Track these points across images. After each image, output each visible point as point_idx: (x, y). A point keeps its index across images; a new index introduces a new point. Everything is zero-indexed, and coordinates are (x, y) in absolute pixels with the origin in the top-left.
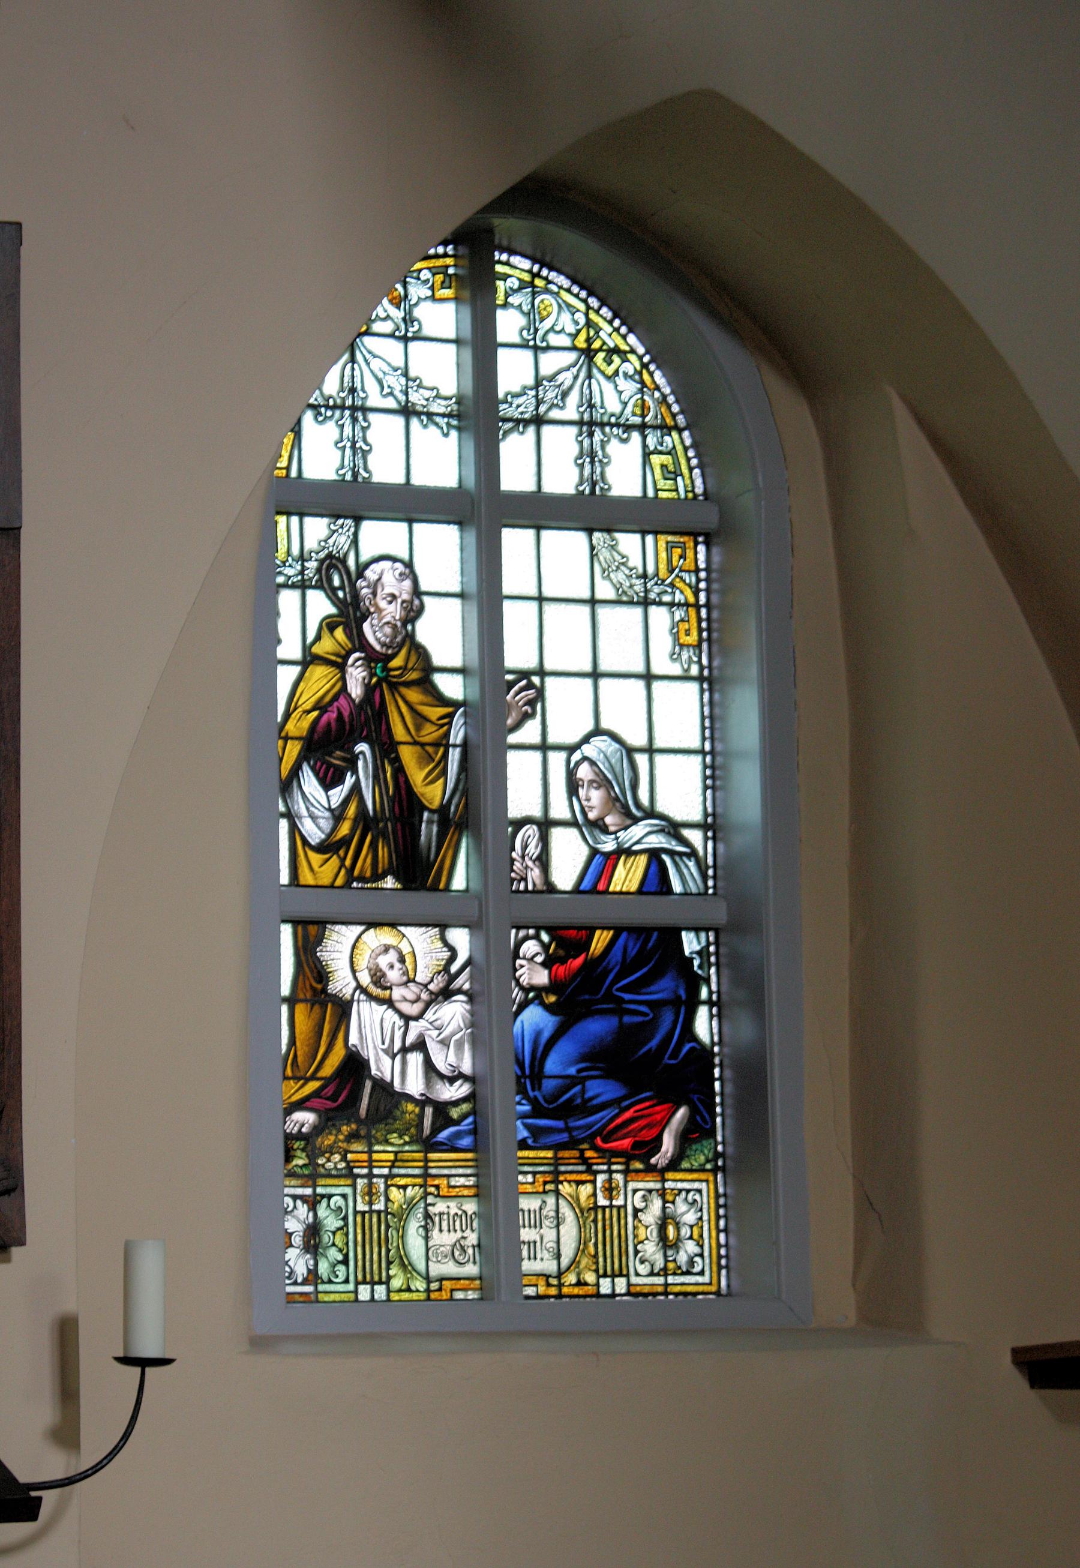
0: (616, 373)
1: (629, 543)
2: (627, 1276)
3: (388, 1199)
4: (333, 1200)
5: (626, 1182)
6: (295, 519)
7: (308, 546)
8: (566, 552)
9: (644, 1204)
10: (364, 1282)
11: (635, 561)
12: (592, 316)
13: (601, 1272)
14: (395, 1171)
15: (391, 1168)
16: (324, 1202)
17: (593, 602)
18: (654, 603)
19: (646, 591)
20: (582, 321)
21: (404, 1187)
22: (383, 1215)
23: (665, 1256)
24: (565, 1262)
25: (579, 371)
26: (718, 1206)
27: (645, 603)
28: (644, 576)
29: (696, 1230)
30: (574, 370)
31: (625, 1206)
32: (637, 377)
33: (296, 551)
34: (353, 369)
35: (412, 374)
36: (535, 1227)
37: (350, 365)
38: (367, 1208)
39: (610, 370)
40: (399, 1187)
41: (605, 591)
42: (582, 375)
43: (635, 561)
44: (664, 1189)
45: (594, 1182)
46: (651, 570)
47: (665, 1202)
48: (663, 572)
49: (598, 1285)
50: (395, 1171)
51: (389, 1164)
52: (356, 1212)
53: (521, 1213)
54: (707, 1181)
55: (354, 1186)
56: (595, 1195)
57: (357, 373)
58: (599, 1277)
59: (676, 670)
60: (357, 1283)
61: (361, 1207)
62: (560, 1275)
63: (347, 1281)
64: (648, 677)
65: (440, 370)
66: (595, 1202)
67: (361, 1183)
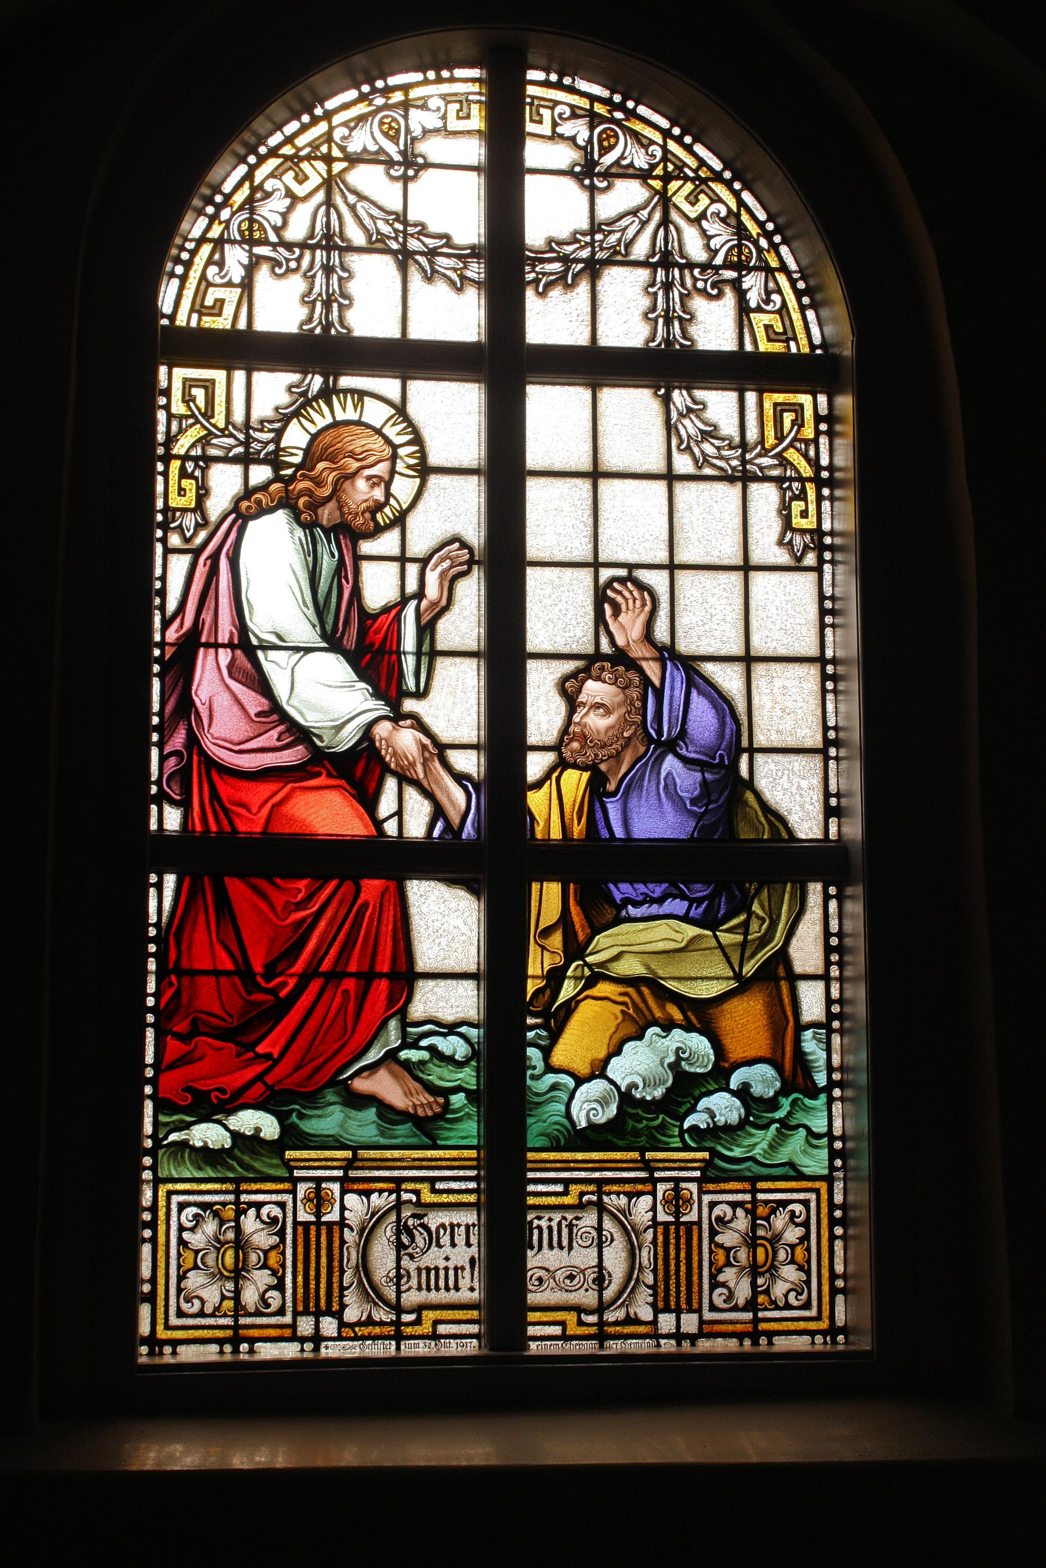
0: (703, 215)
1: (720, 405)
2: (699, 1311)
3: (343, 1208)
4: (265, 1211)
5: (701, 1192)
6: (239, 376)
7: (256, 414)
8: (632, 417)
9: (265, 1218)
10: (306, 1312)
11: (729, 428)
12: (672, 146)
13: (661, 1304)
14: (352, 1174)
15: (346, 1169)
16: (252, 1212)
17: (670, 477)
18: (756, 479)
19: (744, 462)
20: (659, 153)
21: (367, 1193)
22: (336, 1228)
23: (754, 1285)
24: (608, 1294)
25: (650, 214)
26: (833, 1222)
27: (744, 478)
28: (744, 445)
29: (799, 1251)
30: (645, 213)
31: (699, 1223)
32: (732, 221)
33: (238, 417)
34: (328, 215)
35: (411, 217)
36: (561, 1247)
37: (324, 208)
38: (671, 1219)
39: (693, 212)
40: (359, 1192)
41: (683, 464)
42: (657, 216)
43: (729, 428)
44: (754, 1201)
45: (653, 1193)
46: (752, 434)
47: (755, 1218)
48: (770, 440)
49: (655, 1322)
50: (352, 1174)
51: (343, 1164)
52: (296, 1223)
53: (536, 1232)
54: (817, 1191)
55: (293, 1192)
56: (654, 1209)
57: (334, 216)
58: (657, 1311)
59: (783, 557)
60: (296, 1314)
61: (303, 1216)
62: (601, 1308)
63: (281, 1312)
64: (746, 568)
65: (453, 206)
66: (655, 1217)
67: (302, 1188)
